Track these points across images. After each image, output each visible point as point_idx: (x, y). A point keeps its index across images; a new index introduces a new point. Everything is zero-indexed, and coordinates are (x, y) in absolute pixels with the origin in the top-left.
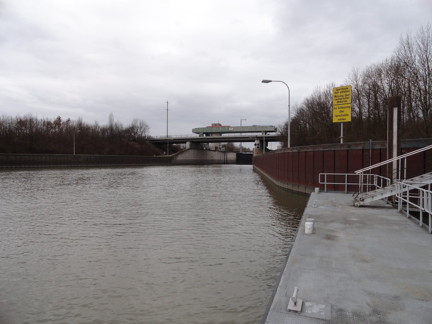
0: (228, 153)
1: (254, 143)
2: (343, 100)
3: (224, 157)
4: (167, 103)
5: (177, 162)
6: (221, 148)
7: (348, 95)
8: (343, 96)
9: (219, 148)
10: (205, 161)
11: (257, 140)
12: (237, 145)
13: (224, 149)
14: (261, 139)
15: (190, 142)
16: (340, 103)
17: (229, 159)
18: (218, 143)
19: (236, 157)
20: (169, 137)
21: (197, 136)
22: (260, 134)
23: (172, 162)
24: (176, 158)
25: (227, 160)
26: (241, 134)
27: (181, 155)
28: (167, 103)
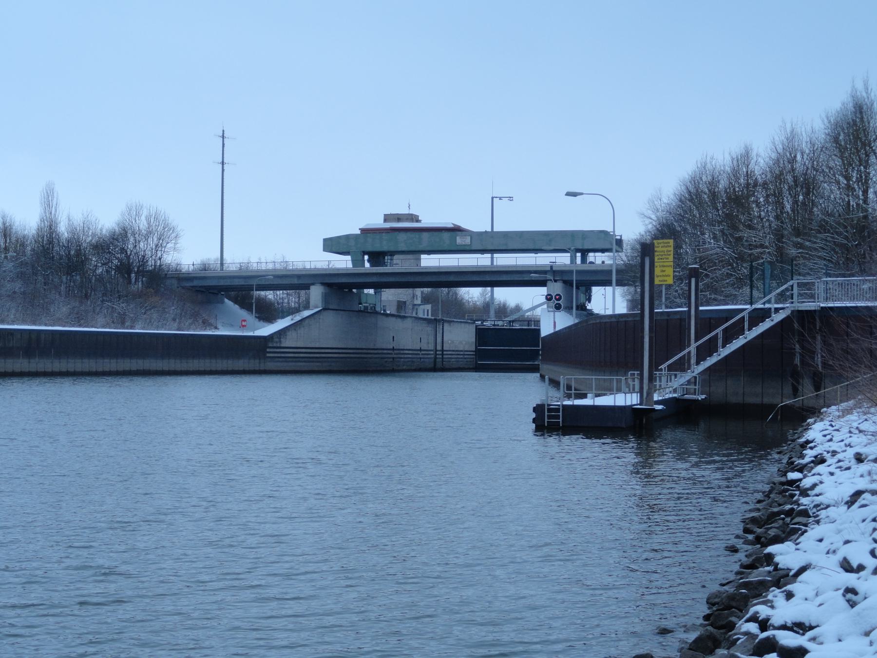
0: (446, 326)
1: (543, 291)
2: (664, 257)
3: (432, 339)
4: (223, 137)
5: (283, 355)
6: (420, 305)
7: (670, 251)
8: (664, 251)
9: (411, 307)
10: (372, 351)
11: (556, 281)
12: (473, 295)
13: (428, 311)
14: (566, 278)
15: (323, 284)
16: (661, 261)
17: (451, 349)
18: (410, 291)
19: (474, 340)
20: (225, 266)
21: (343, 262)
22: (563, 259)
23: (268, 355)
24: (280, 342)
25: (443, 350)
26: (492, 258)
27: (295, 330)
28: (223, 137)
